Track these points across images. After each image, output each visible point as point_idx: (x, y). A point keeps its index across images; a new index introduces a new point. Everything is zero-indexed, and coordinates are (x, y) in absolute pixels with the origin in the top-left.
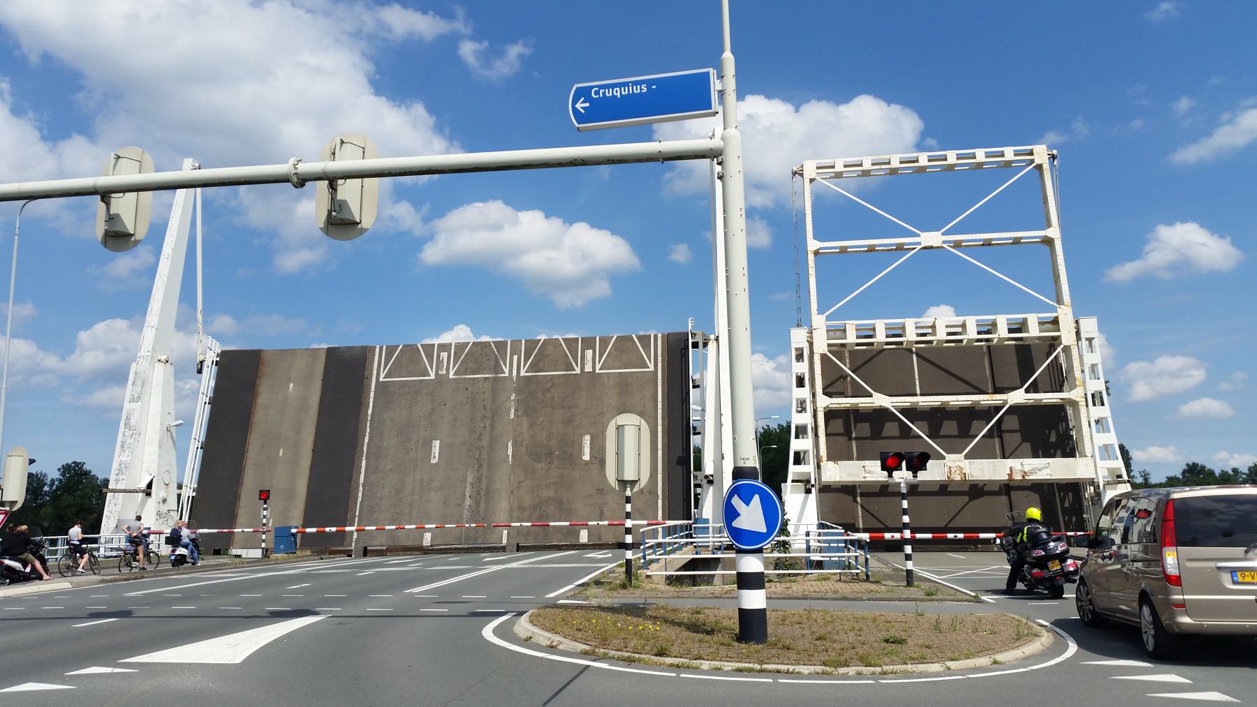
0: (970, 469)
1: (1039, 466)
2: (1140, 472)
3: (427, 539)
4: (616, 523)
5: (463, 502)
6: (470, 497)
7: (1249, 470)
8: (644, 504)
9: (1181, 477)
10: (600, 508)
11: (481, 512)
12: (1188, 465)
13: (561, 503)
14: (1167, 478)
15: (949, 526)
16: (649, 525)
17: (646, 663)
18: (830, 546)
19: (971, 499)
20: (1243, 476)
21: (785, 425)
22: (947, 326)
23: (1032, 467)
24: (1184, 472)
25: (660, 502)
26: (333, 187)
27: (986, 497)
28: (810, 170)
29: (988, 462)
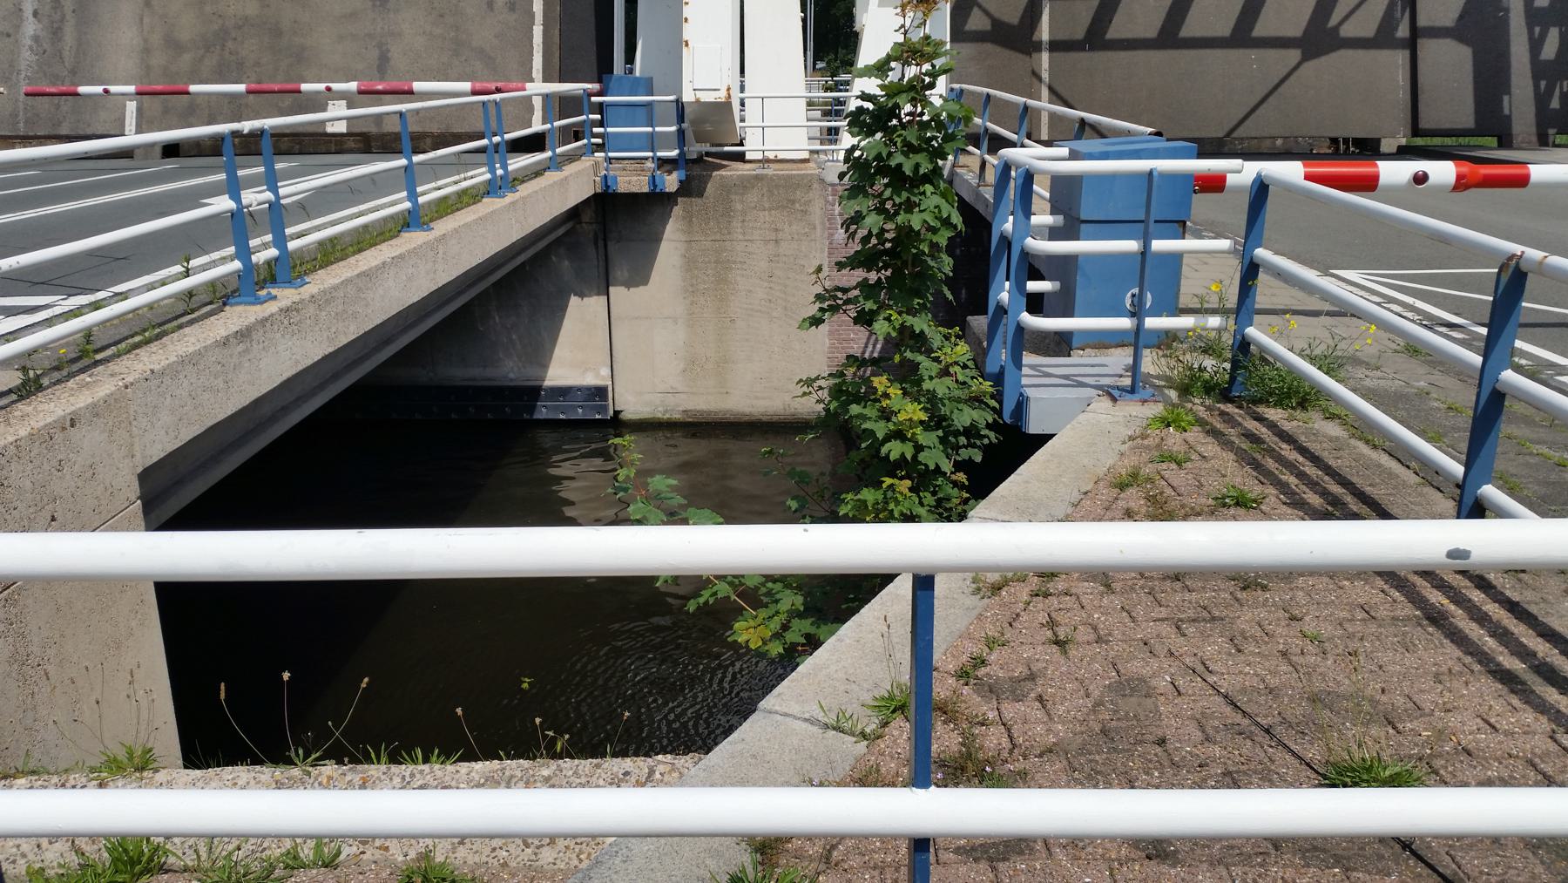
3: (538, 52)
4: (380, 87)
5: (18, 27)
6: (35, 14)
8: (496, 37)
10: (380, 45)
11: (66, 54)
13: (277, 32)
16: (474, 93)
19: (1306, 58)
25: (538, 31)
27: (1342, 52)
28: (1019, 574)
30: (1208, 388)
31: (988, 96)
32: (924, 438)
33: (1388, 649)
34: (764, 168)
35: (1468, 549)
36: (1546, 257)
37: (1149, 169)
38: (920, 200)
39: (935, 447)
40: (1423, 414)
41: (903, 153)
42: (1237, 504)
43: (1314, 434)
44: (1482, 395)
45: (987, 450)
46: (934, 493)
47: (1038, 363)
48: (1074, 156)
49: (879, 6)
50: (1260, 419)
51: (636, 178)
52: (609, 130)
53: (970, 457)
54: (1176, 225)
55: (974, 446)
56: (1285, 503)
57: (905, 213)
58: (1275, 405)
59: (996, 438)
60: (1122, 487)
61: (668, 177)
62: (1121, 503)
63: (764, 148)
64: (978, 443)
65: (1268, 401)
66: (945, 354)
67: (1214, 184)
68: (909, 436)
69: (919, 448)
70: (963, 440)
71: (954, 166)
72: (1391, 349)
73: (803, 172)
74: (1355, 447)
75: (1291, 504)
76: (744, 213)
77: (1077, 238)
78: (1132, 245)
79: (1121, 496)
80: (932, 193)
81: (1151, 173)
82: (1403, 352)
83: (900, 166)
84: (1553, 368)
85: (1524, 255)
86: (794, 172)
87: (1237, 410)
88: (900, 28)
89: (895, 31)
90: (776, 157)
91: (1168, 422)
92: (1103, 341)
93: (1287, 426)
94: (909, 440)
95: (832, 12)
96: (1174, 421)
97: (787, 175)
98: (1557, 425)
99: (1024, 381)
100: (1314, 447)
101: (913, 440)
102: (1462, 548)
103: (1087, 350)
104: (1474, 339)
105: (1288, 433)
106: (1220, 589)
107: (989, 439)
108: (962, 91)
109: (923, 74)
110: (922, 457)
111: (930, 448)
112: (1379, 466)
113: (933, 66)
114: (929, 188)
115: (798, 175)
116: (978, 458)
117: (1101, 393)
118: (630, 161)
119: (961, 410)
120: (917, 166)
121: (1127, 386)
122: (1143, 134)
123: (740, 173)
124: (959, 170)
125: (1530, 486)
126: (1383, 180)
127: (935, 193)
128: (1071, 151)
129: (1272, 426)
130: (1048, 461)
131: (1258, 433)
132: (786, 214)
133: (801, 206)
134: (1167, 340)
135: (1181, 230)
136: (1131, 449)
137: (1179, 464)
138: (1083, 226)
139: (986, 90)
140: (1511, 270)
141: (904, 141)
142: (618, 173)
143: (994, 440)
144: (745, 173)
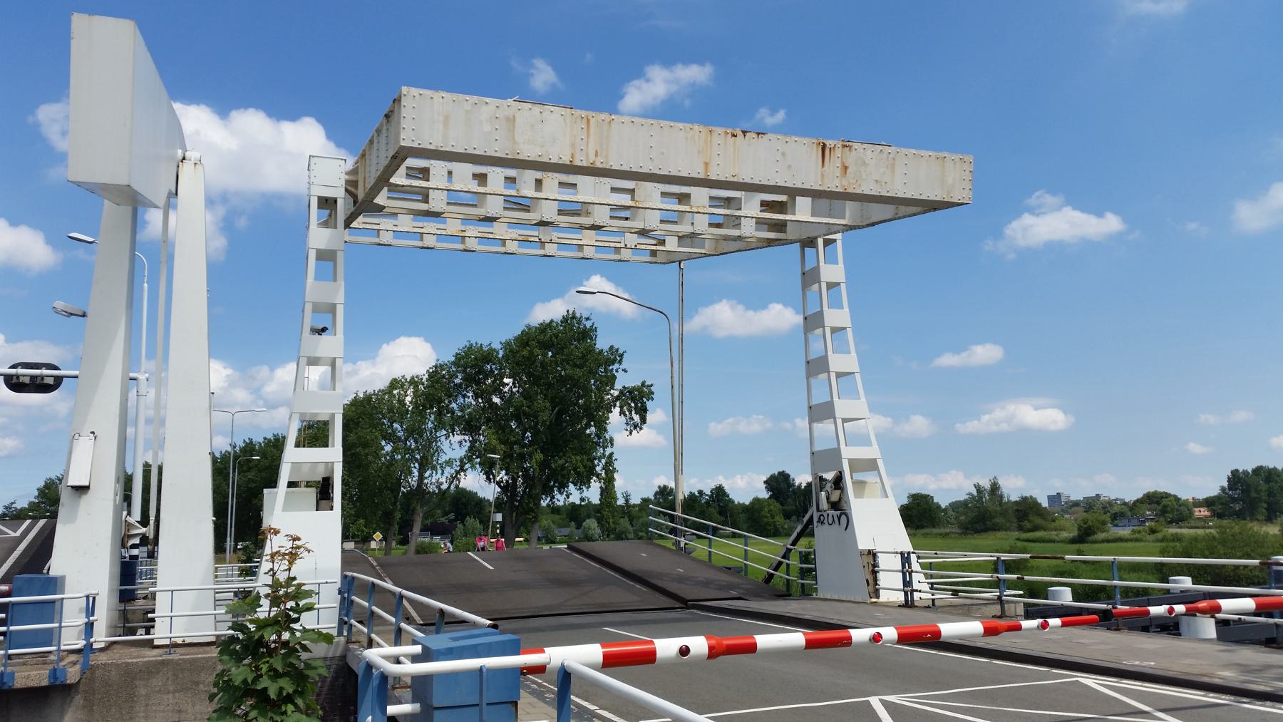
2: (622, 494)
7: (711, 492)
9: (653, 498)
12: (659, 487)
14: (642, 499)
17: (1038, 568)
20: (707, 497)
22: (160, 469)
24: (656, 494)
26: (1269, 568)
31: (373, 584)
34: (170, 654)
37: (479, 666)
41: (270, 677)
48: (426, 656)
49: (283, 511)
51: (35, 673)
52: (12, 628)
54: (510, 705)
61: (70, 670)
63: (171, 635)
67: (539, 669)
73: (208, 656)
76: (148, 697)
80: (292, 712)
81: (481, 669)
83: (265, 689)
86: (199, 656)
88: (269, 571)
89: (266, 573)
90: (184, 641)
95: (254, 502)
97: (193, 658)
108: (353, 578)
109: (287, 609)
113: (297, 605)
114: (290, 708)
115: (203, 658)
118: (34, 656)
120: (281, 689)
123: (146, 659)
126: (659, 654)
128: (425, 648)
132: (189, 695)
133: (204, 686)
135: (514, 709)
138: (436, 713)
139: (371, 579)
141: (272, 669)
142: (14, 669)
144: (151, 659)
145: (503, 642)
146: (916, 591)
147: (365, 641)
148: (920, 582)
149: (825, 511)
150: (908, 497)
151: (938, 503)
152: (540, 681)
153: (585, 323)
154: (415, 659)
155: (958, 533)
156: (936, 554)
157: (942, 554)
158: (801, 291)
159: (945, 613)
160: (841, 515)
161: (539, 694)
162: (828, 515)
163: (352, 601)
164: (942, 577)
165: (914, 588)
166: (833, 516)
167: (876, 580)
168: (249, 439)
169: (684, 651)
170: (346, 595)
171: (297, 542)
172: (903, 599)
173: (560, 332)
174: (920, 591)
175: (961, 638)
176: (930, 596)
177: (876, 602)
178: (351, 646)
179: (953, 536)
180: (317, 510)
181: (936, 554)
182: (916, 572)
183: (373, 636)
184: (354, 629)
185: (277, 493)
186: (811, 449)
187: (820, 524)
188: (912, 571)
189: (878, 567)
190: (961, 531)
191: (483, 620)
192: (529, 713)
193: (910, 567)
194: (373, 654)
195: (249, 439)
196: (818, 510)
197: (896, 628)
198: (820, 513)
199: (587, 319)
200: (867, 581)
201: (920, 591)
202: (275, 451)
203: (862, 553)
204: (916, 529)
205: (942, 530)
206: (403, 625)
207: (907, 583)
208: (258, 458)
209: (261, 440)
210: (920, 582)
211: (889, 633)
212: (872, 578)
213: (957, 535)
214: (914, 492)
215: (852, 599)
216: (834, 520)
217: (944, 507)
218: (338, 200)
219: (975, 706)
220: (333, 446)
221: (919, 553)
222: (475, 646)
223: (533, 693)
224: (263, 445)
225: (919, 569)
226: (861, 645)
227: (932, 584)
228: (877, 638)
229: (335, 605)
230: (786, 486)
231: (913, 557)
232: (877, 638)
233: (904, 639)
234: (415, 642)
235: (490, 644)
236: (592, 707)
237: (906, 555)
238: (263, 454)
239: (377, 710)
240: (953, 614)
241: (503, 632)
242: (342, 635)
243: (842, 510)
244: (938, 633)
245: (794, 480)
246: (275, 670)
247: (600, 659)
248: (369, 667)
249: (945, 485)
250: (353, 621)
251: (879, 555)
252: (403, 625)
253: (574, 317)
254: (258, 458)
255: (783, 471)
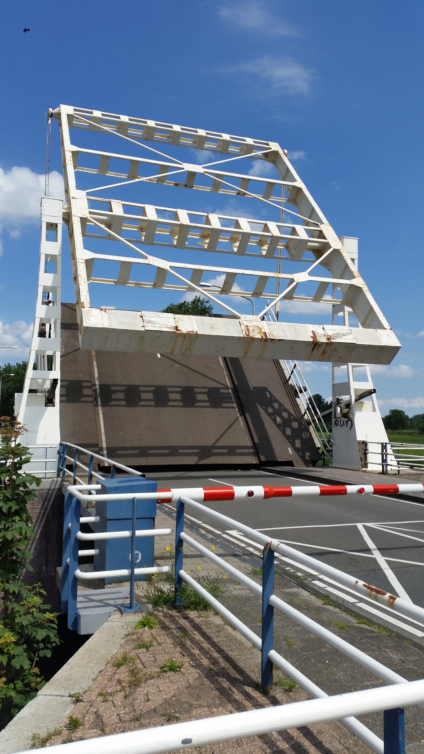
0: (269, 329)
1: (342, 332)
15: (216, 445)
18: (133, 535)
21: (21, 364)
23: (334, 332)
29: (287, 325)
30: (166, 602)
32: (14, 650)
33: (230, 747)
35: (190, 738)
36: (279, 544)
38: (12, 524)
39: (21, 655)
40: (256, 608)
42: (170, 670)
43: (209, 624)
44: (264, 608)
45: (55, 650)
46: (22, 681)
47: (88, 594)
48: (103, 491)
50: (186, 618)
53: (45, 655)
54: (150, 519)
55: (47, 648)
56: (192, 666)
57: (4, 531)
58: (194, 610)
59: (60, 642)
60: (118, 665)
62: (117, 677)
64: (50, 646)
65: (190, 607)
66: (28, 602)
67: (168, 500)
68: (6, 651)
69: (11, 657)
70: (42, 645)
71: (62, 481)
72: (246, 573)
74: (226, 630)
75: (195, 666)
77: (105, 531)
78: (126, 534)
79: (117, 671)
80: (19, 520)
82: (251, 574)
84: (311, 577)
85: (272, 543)
87: (177, 614)
91: (145, 624)
92: (119, 580)
93: (198, 621)
94: (6, 654)
96: (147, 624)
98: (310, 608)
99: (79, 605)
100: (208, 632)
101: (8, 653)
102: (188, 738)
103: (113, 584)
104: (281, 564)
105: (198, 625)
106: (157, 723)
107: (56, 643)
110: (13, 662)
111: (19, 656)
112: (236, 639)
113: (21, 459)
114: (17, 518)
116: (49, 655)
117: (116, 609)
119: (37, 632)
120: (10, 508)
121: (128, 604)
122: (137, 475)
124: (64, 483)
125: (297, 643)
126: (236, 495)
127: (20, 521)
128: (103, 486)
129: (191, 621)
130: (84, 654)
131: (184, 626)
134: (148, 578)
135: (153, 522)
136: (126, 641)
137: (147, 649)
138: (109, 522)
140: (268, 550)
143: (58, 643)
145: (148, 484)
146: (389, 465)
147: (72, 480)
148: (391, 460)
149: (339, 418)
150: (390, 412)
151: (407, 415)
152: (170, 507)
153: (205, 304)
154: (98, 492)
155: (418, 433)
156: (402, 445)
157: (405, 445)
158: (332, 290)
159: (405, 478)
160: (348, 420)
161: (169, 514)
162: (341, 420)
163: (65, 458)
164: (406, 458)
165: (388, 463)
166: (343, 421)
167: (366, 458)
168: (8, 363)
169: (251, 494)
170: (62, 455)
171: (19, 425)
172: (381, 469)
173: (190, 308)
174: (391, 465)
175: (414, 492)
176: (397, 468)
177: (365, 470)
178: (64, 483)
179: (415, 434)
180: (45, 406)
181: (402, 445)
182: (390, 454)
183: (77, 478)
184: (66, 474)
185: (22, 396)
186: (333, 382)
187: (335, 426)
188: (387, 454)
189: (368, 451)
190: (419, 432)
191: (137, 472)
192: (163, 524)
193: (386, 451)
194: (73, 489)
195: (8, 363)
196: (335, 417)
197: (373, 486)
198: (336, 419)
199: (207, 302)
200: (361, 458)
201: (391, 465)
202: (23, 371)
203: (359, 442)
204: (393, 430)
205: (409, 431)
206: (93, 473)
207: (384, 460)
208: (14, 375)
209: (15, 365)
210: (391, 460)
211: (369, 488)
212: (364, 457)
213: (417, 434)
214: (393, 409)
215: (352, 468)
216: (344, 424)
217: (410, 418)
218: (58, 225)
219: (418, 531)
220: (55, 370)
221: (392, 444)
222: (131, 487)
223: (166, 513)
224: (16, 367)
225: (392, 453)
226: (352, 494)
227: (398, 461)
228: (361, 491)
229: (56, 460)
230: (319, 403)
231: (389, 446)
232: (361, 491)
233: (377, 491)
234: (98, 483)
235: (140, 485)
236: (199, 522)
237: (384, 445)
238: (17, 373)
239: (74, 520)
240: (409, 479)
241: (148, 479)
242: (60, 477)
243: (349, 418)
244: (397, 490)
245: (324, 400)
246: (7, 497)
247: (203, 496)
248: (71, 496)
249: (413, 405)
250: (65, 469)
251: (368, 444)
252: (93, 473)
253: (199, 300)
254: (14, 375)
255: (319, 394)
